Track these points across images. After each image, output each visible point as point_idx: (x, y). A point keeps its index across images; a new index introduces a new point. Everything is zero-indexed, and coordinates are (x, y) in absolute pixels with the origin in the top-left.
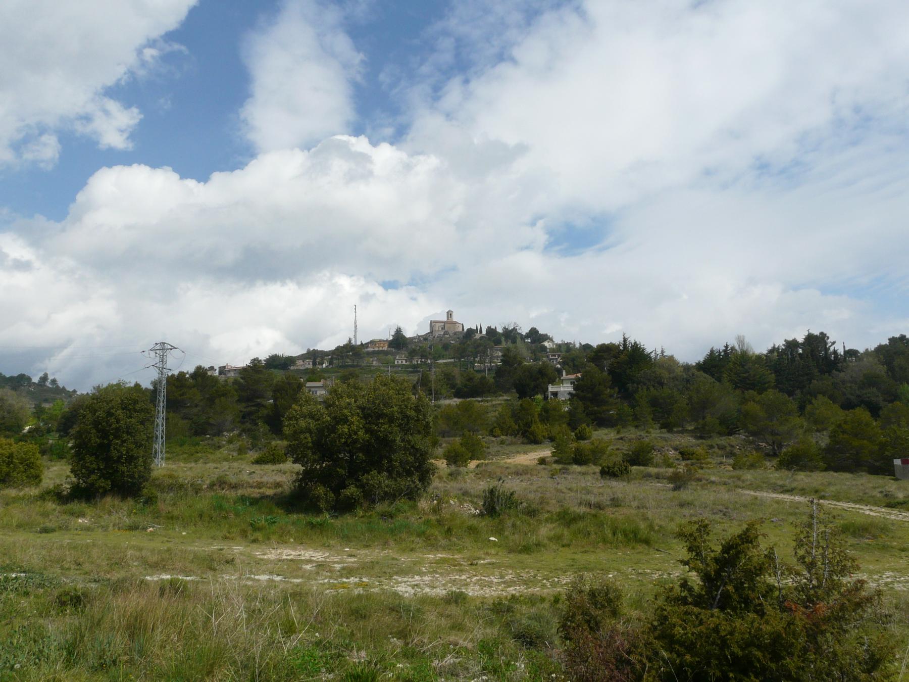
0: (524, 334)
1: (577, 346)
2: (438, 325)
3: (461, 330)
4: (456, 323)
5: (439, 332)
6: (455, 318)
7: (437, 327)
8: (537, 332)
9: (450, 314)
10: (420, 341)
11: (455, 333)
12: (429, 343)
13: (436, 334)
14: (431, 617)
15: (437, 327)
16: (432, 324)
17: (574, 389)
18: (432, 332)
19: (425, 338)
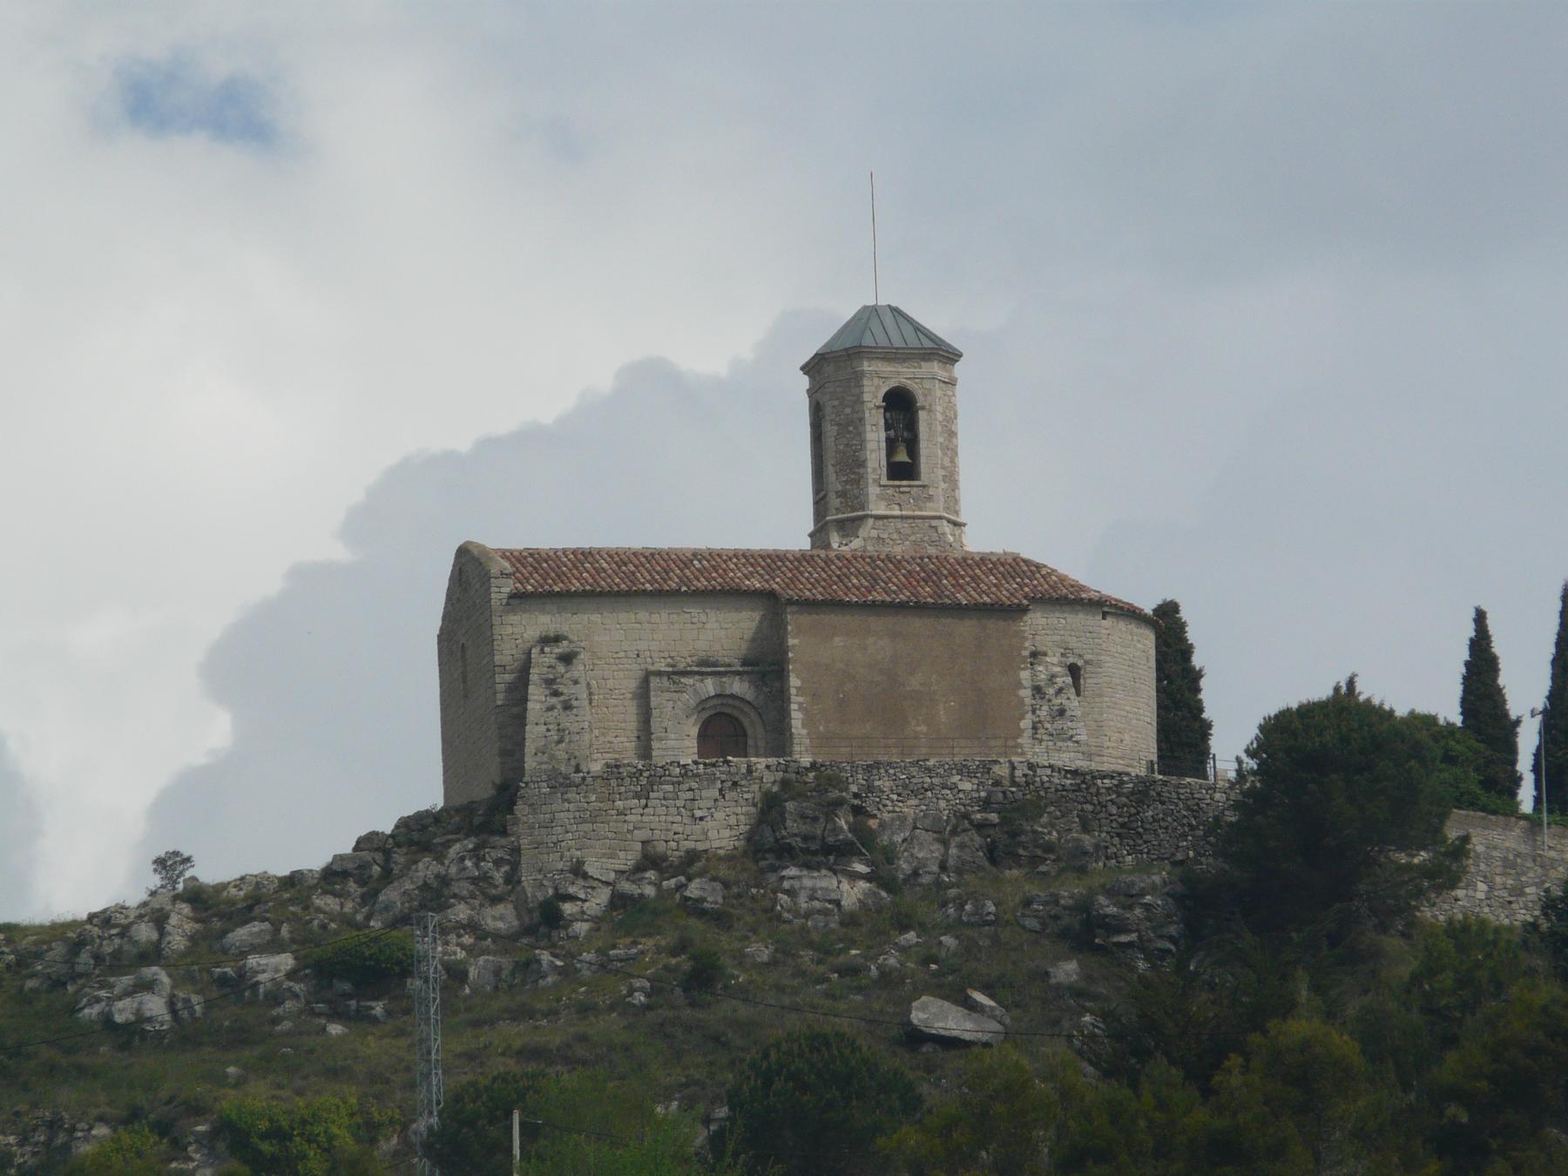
0: (805, 544)
1: (1362, 698)
2: (618, 643)
3: (1123, 735)
4: (1018, 593)
5: (643, 804)
6: (1004, 495)
7: (609, 688)
8: (1177, 612)
9: (874, 402)
10: (228, 1013)
11: (1009, 825)
12: (432, 1063)
13: (590, 851)
14: (778, 684)
15: (609, 688)
16: (502, 620)
17: (1465, 933)
18: (486, 805)
19: (345, 938)
